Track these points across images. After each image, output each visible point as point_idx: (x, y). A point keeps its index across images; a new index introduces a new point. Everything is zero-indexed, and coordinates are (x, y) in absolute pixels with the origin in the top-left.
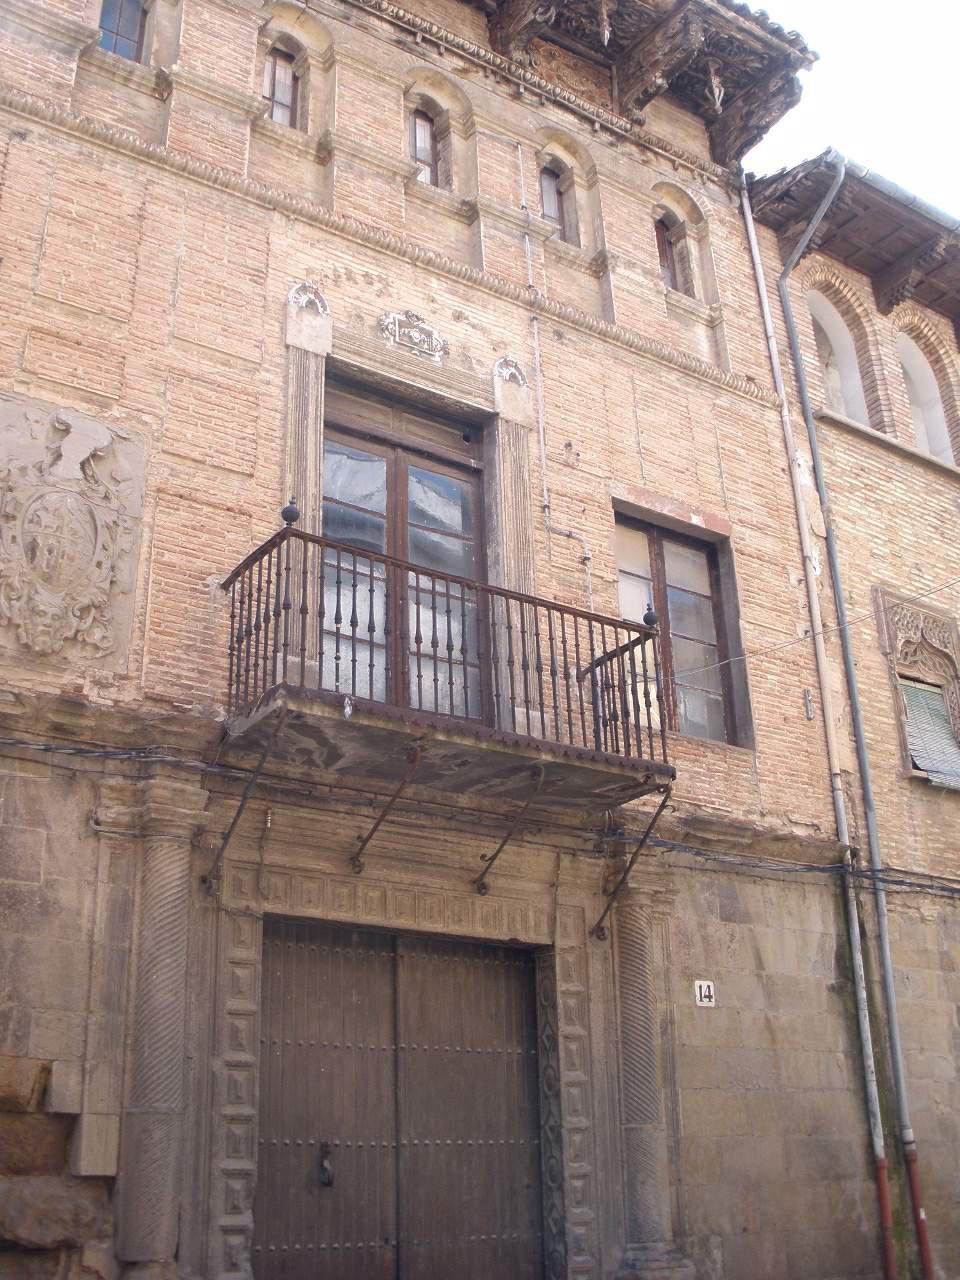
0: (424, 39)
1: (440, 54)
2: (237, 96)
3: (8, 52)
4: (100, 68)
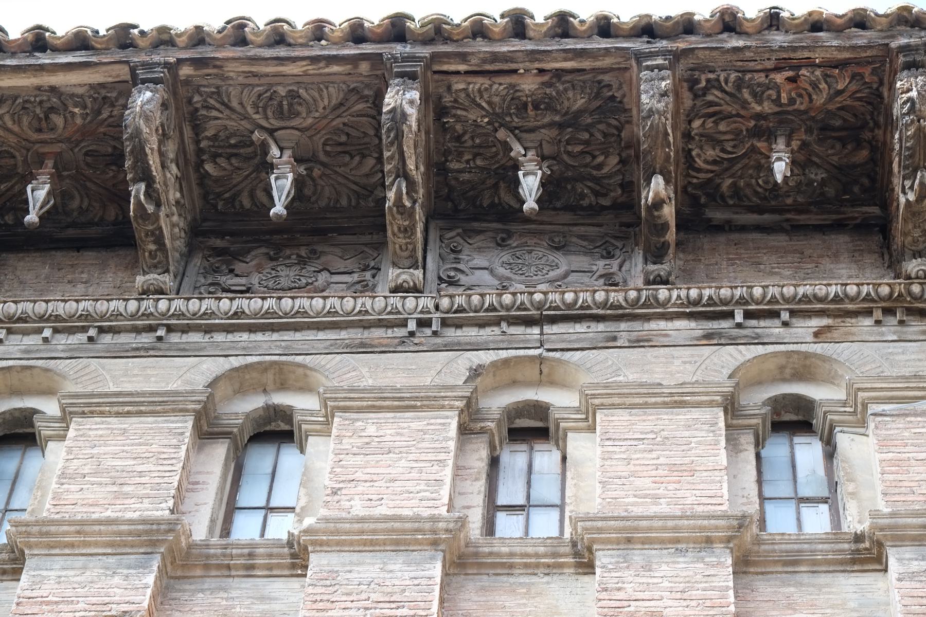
0: (748, 315)
1: (785, 324)
2: (408, 526)
3: (50, 598)
4: (207, 567)
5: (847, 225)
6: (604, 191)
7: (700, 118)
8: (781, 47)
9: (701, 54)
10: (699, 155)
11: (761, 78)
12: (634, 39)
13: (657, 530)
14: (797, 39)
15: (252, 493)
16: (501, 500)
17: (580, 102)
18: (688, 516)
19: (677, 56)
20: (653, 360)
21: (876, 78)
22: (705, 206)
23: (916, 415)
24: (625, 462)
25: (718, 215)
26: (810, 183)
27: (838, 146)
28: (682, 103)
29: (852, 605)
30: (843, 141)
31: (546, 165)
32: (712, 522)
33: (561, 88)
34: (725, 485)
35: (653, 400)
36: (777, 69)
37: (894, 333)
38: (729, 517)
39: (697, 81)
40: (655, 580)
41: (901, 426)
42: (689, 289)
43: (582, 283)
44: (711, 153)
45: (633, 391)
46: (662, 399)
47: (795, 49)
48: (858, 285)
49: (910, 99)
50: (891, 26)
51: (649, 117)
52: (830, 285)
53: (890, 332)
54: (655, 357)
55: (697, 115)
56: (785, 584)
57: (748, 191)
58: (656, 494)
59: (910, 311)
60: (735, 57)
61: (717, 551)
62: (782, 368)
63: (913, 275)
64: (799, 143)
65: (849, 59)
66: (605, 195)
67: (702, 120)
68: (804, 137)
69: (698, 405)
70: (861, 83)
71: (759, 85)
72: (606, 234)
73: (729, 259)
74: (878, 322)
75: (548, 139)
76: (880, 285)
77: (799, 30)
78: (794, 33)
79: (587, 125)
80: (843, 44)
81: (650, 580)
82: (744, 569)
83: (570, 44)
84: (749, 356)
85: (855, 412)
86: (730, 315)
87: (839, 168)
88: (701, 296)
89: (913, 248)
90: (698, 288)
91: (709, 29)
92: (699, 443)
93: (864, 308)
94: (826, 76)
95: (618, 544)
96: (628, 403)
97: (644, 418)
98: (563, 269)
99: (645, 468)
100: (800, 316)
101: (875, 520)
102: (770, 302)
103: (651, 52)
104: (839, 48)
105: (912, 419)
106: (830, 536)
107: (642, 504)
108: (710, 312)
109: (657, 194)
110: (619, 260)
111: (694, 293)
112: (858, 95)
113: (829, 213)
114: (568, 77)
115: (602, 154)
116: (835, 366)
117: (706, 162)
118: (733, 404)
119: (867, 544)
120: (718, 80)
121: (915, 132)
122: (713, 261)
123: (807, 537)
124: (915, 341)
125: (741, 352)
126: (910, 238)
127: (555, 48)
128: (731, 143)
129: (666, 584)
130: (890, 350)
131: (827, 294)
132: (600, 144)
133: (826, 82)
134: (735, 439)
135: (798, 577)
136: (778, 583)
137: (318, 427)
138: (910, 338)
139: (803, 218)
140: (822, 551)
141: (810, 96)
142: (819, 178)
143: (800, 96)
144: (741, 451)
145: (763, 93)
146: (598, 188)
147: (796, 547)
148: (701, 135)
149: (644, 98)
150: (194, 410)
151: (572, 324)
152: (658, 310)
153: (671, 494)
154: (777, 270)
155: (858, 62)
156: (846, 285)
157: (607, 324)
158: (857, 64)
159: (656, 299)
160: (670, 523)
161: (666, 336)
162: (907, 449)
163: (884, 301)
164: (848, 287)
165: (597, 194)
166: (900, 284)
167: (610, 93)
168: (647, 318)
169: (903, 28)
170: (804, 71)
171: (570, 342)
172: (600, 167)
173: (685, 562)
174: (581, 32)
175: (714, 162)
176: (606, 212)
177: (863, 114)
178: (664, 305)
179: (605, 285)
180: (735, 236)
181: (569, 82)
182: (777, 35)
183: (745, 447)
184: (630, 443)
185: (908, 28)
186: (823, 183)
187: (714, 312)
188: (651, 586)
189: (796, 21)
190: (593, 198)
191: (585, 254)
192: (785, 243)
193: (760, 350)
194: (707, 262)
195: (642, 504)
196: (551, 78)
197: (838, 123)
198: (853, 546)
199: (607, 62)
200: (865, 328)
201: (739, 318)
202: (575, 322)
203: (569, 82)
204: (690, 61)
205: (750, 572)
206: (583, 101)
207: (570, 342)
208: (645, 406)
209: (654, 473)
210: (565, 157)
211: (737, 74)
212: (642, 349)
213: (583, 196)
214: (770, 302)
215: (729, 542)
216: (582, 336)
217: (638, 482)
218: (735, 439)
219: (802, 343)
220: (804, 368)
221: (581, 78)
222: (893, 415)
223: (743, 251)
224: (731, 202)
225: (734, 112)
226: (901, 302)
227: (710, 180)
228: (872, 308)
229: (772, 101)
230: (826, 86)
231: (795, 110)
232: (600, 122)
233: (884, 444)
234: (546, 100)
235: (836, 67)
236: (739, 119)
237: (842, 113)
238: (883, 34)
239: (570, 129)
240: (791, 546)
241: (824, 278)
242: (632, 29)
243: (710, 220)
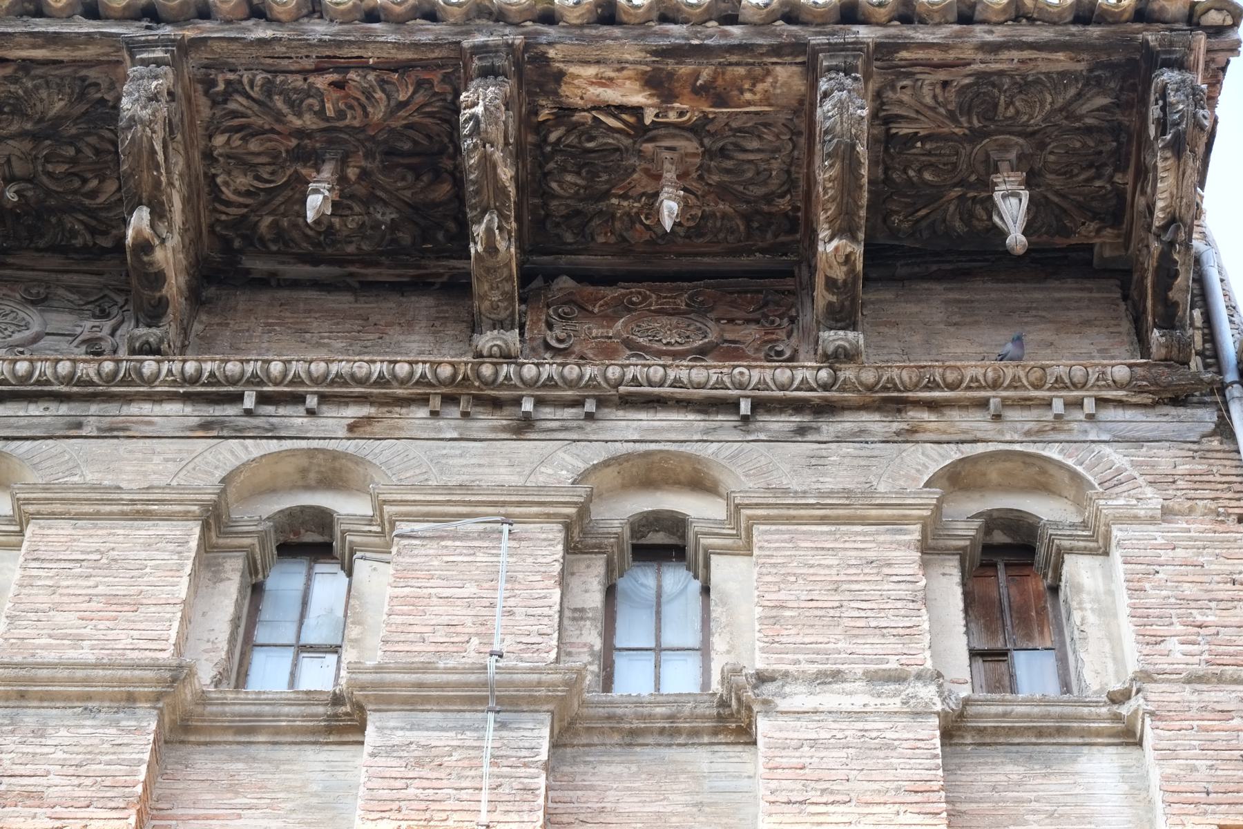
0: (263, 399)
1: (311, 413)
5: (433, 284)
6: (103, 228)
7: (223, 132)
8: (320, 40)
9: (216, 46)
10: (226, 184)
11: (297, 82)
12: (130, 22)
13: (62, 682)
14: (344, 31)
15: (277, 626)
16: (619, 642)
17: (59, 105)
18: (104, 665)
19: (184, 48)
20: (126, 455)
21: (448, 88)
22: (241, 251)
23: (455, 538)
24: (50, 591)
25: (259, 265)
26: (376, 226)
27: (410, 177)
28: (198, 111)
29: (315, 787)
30: (417, 172)
31: (14, 189)
32: (137, 673)
33: (30, 85)
34: (176, 625)
35: (108, 508)
36: (319, 70)
37: (455, 428)
38: (159, 667)
39: (213, 83)
40: (46, 750)
41: (431, 552)
42: (185, 361)
43: (56, 350)
44: (243, 181)
45: (82, 496)
46: (120, 507)
47: (339, 44)
48: (410, 363)
49: (474, 117)
50: (468, 18)
51: (130, 127)
52: (374, 362)
53: (449, 427)
54: (130, 452)
55: (218, 128)
56: (233, 758)
57: (295, 234)
58: (78, 635)
59: (480, 400)
60: (262, 53)
61: (140, 712)
62: (304, 472)
63: (485, 353)
64: (357, 171)
65: (414, 60)
66: (105, 233)
67: (227, 135)
68: (363, 163)
69: (169, 517)
70: (430, 92)
71: (295, 90)
72: (106, 286)
73: (267, 324)
74: (434, 414)
75: (19, 153)
76: (440, 363)
77: (347, 18)
78: (341, 23)
79: (72, 137)
80: (402, 40)
81: (38, 750)
82: (182, 738)
83: (41, 26)
84: (256, 453)
85: (383, 532)
86: (238, 398)
87: (414, 207)
88: (200, 372)
89: (493, 316)
90: (197, 360)
91: (229, 13)
92: (156, 568)
93: (419, 394)
94: (382, 83)
95: (7, 700)
96: (73, 511)
97: (91, 532)
98: (35, 328)
99: (74, 599)
100: (334, 403)
101: (354, 676)
102: (292, 383)
103: (147, 41)
104: (397, 46)
105: (449, 543)
106: (300, 696)
107: (56, 647)
108: (212, 393)
109: (138, 233)
110: (113, 321)
111: (190, 367)
112: (427, 109)
113: (406, 266)
114: (40, 71)
115: (96, 177)
116: (371, 471)
117: (237, 192)
118: (218, 518)
119: (348, 709)
120: (240, 82)
121: (479, 160)
122: (245, 326)
123: (270, 696)
124: (481, 440)
125: (246, 448)
126: (487, 303)
127: (18, 30)
128: (269, 169)
129: (60, 755)
130: (444, 452)
131: (370, 374)
132: (91, 163)
133: (384, 91)
134: (219, 564)
135: (253, 750)
136: (223, 757)
137: (729, 542)
138: (475, 435)
139: (371, 273)
140: (287, 716)
141: (364, 108)
142: (388, 218)
143: (351, 107)
144: (222, 580)
145: (302, 102)
146: (94, 223)
147: (253, 709)
148: (228, 156)
149: (125, 103)
150: (920, 518)
151: (24, 405)
152: (141, 389)
153: (99, 634)
154: (326, 341)
155: (426, 66)
156: (396, 362)
157: (72, 405)
158: (425, 67)
159: (140, 373)
160: (80, 674)
161: (150, 423)
162: (432, 583)
163: (446, 386)
164: (398, 366)
165: (93, 232)
166: (466, 363)
167: (99, 95)
168: (128, 399)
169: (484, 21)
170: (352, 75)
171: (18, 428)
172: (94, 194)
173: (92, 727)
174: (57, 9)
175: (248, 193)
176: (109, 256)
177: (438, 135)
178: (150, 381)
179: (87, 353)
180: (284, 294)
181: (41, 77)
182: (318, 24)
183: (228, 575)
184: (63, 565)
185: (491, 23)
186: (394, 226)
187: (217, 394)
188: (38, 757)
189: (341, 7)
190: (88, 237)
191: (72, 311)
192: (346, 306)
193: (274, 446)
194: (236, 328)
195: (56, 647)
196: (16, 71)
197: (407, 146)
198: (330, 710)
199: (91, 52)
200: (417, 421)
201: (249, 402)
202: (30, 402)
203: (41, 77)
204: (203, 56)
205: (189, 742)
206: (62, 103)
207: (18, 428)
208: (97, 516)
209: (84, 606)
210: (45, 179)
211: (265, 75)
212: (116, 441)
213: (74, 234)
214: (292, 383)
215: (158, 700)
216: (35, 420)
217: (59, 618)
218: (219, 564)
219: (331, 438)
220: (335, 474)
221: (57, 72)
222: (425, 538)
223: (288, 314)
224: (274, 248)
225: (267, 127)
226: (467, 387)
227: (244, 216)
228: (429, 394)
229: (315, 113)
230: (384, 96)
231: (347, 127)
232: (88, 134)
233: (401, 578)
234: (11, 101)
235: (395, 71)
236: (276, 136)
237: (410, 132)
238: (457, 29)
239: (48, 142)
240: (248, 707)
241: (386, 353)
242: (125, 8)
243: (248, 271)
